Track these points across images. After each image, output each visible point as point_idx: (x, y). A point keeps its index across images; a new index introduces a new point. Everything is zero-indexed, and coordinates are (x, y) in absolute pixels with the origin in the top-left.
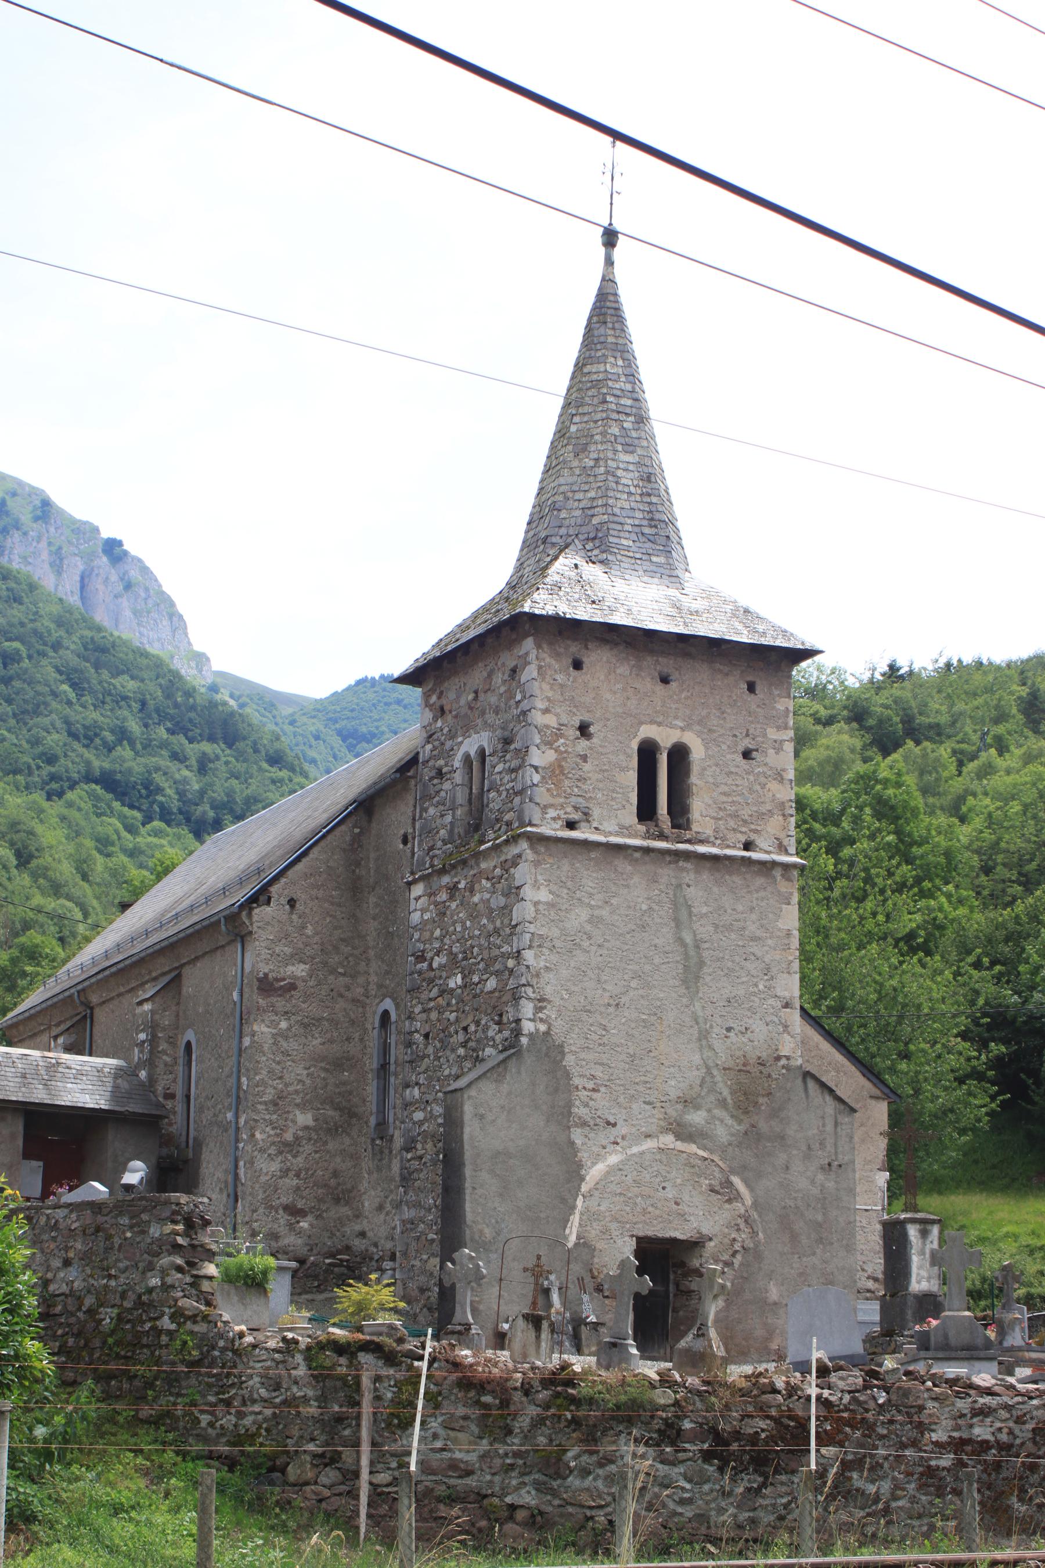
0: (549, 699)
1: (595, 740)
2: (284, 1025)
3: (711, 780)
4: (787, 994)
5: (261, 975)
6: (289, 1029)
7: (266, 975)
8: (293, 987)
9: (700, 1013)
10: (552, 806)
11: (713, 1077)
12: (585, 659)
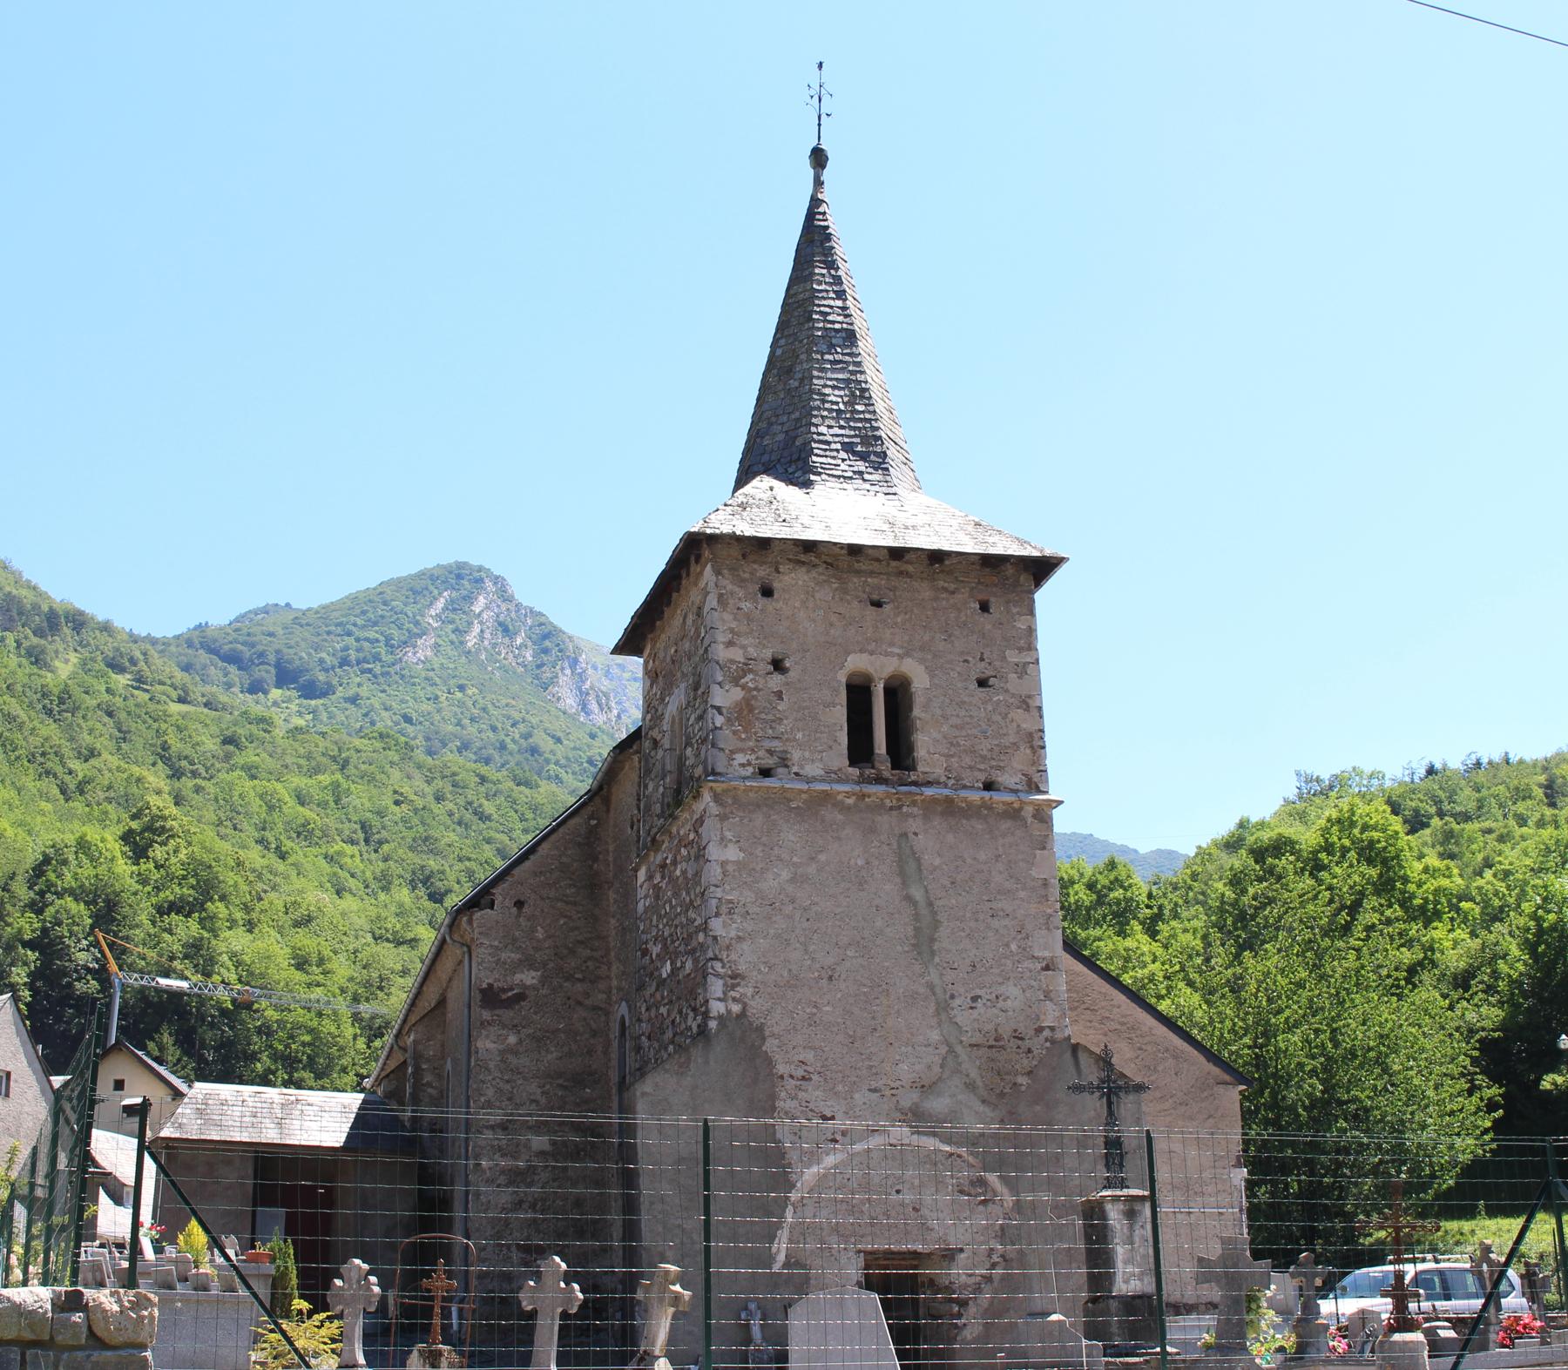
0: (732, 631)
1: (791, 674)
2: (512, 1039)
3: (939, 712)
4: (1047, 954)
5: (484, 986)
6: (520, 1042)
7: (490, 986)
8: (521, 997)
9: (937, 981)
10: (742, 750)
11: (957, 1056)
12: (776, 585)
